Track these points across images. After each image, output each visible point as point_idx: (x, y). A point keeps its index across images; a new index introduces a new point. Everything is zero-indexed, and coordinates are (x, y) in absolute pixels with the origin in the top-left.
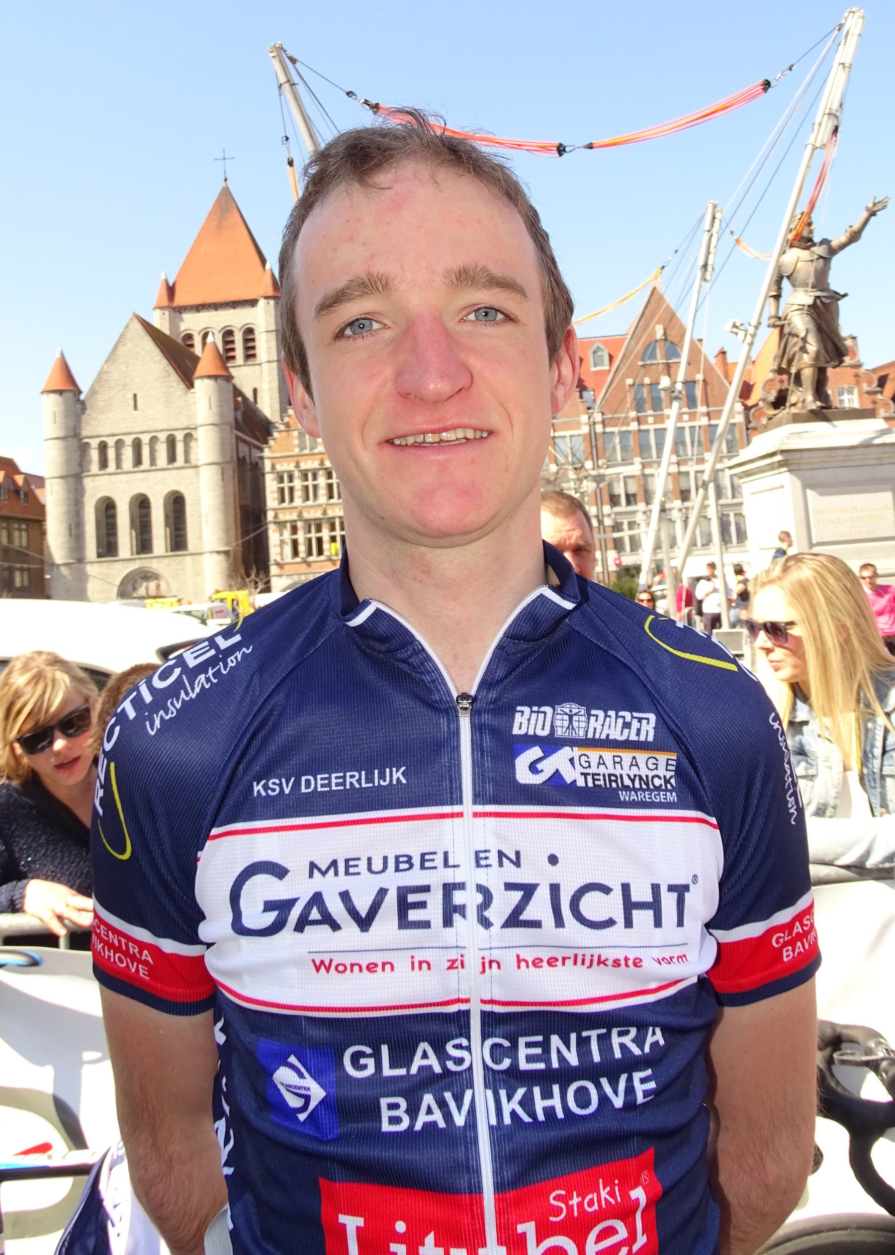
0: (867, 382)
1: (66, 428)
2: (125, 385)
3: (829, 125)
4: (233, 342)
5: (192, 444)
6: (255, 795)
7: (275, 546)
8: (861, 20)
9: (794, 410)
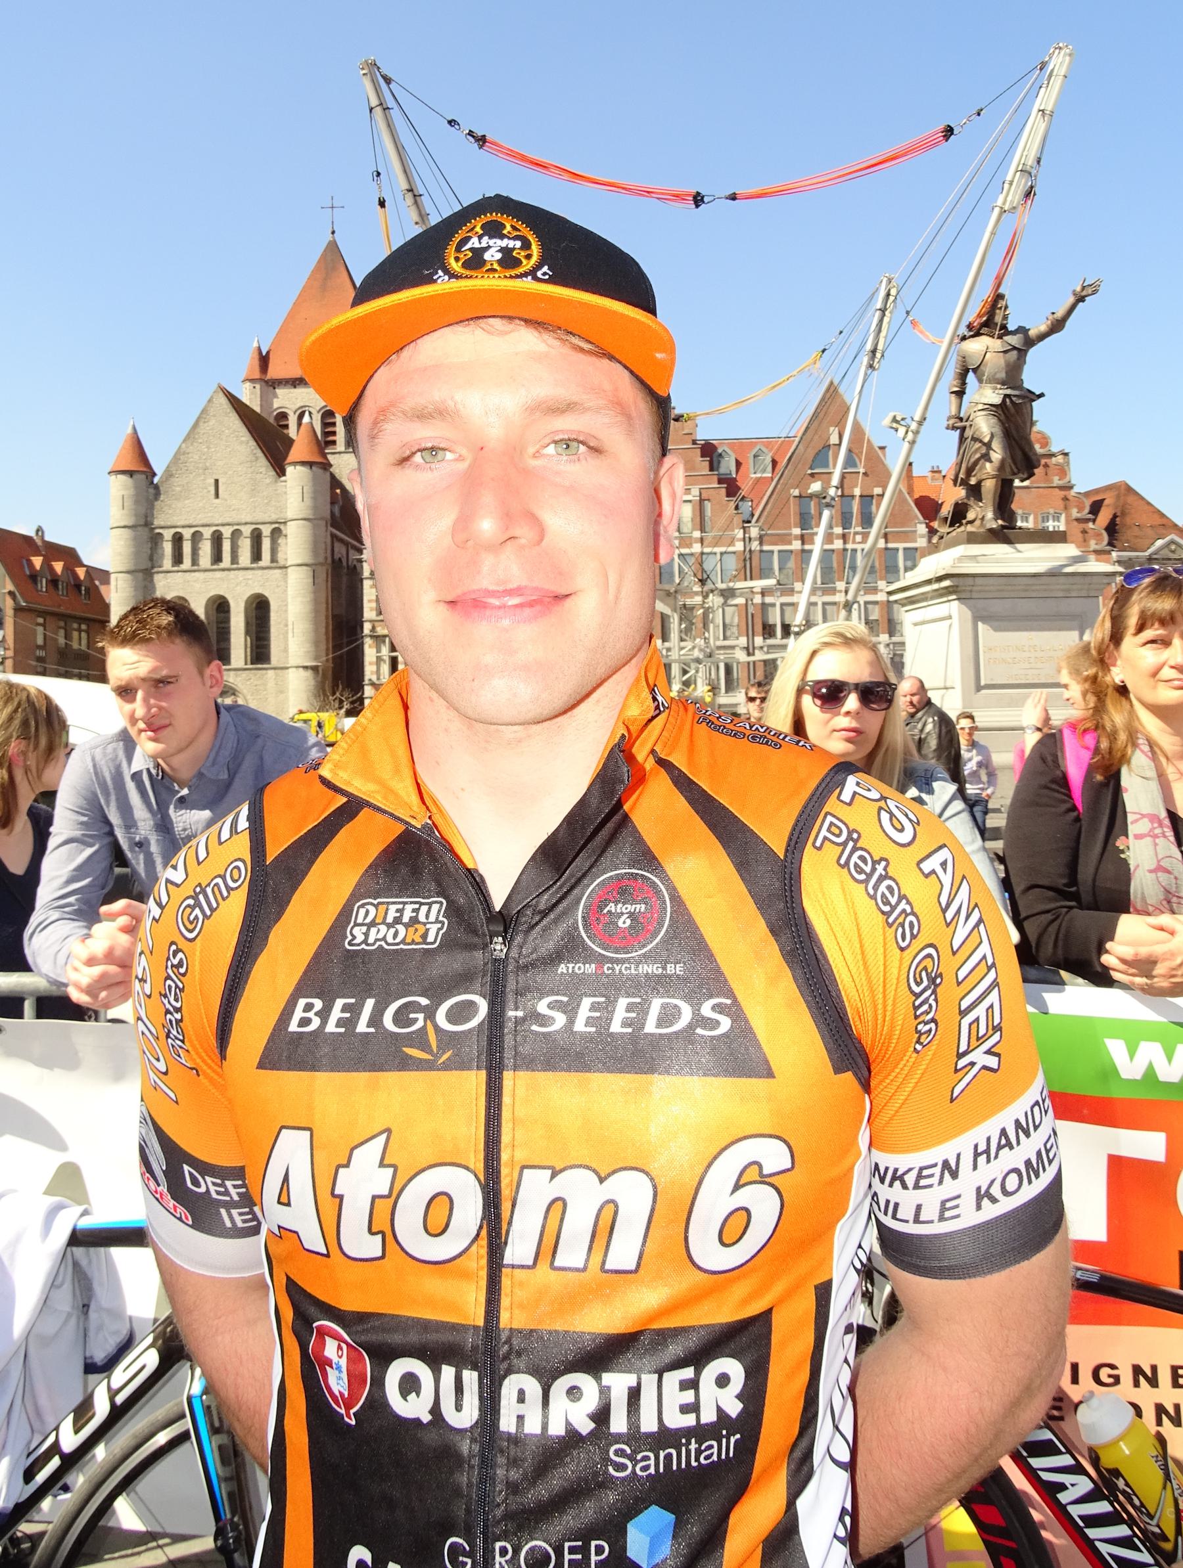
0: (1077, 507)
1: (136, 515)
3: (1021, 185)
6: (412, 1016)
7: (370, 664)
8: (1068, 58)
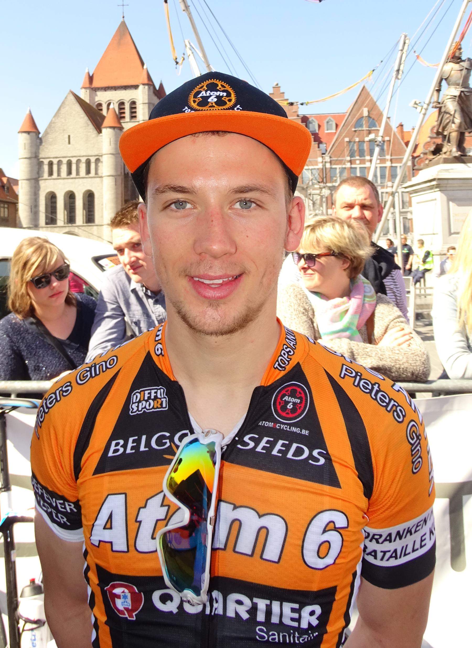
1: (31, 153)
2: (64, 130)
4: (124, 109)
5: (100, 164)
9: (444, 156)
